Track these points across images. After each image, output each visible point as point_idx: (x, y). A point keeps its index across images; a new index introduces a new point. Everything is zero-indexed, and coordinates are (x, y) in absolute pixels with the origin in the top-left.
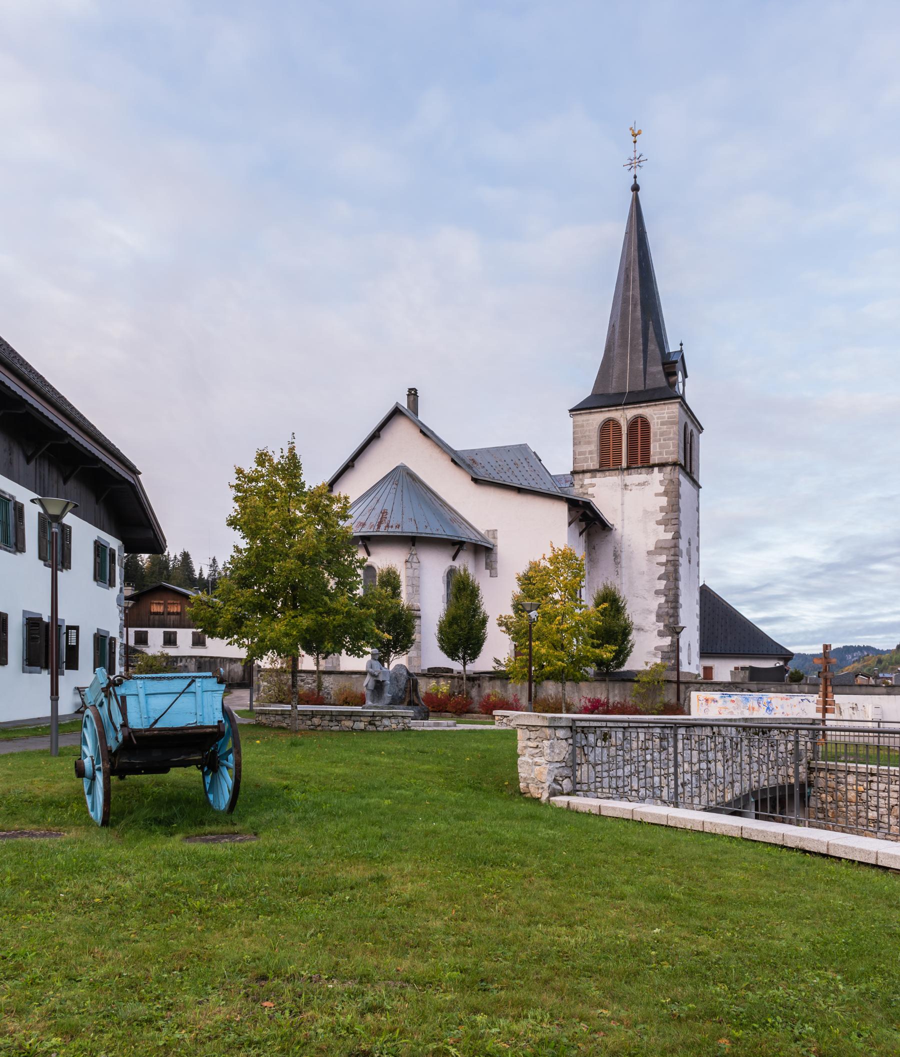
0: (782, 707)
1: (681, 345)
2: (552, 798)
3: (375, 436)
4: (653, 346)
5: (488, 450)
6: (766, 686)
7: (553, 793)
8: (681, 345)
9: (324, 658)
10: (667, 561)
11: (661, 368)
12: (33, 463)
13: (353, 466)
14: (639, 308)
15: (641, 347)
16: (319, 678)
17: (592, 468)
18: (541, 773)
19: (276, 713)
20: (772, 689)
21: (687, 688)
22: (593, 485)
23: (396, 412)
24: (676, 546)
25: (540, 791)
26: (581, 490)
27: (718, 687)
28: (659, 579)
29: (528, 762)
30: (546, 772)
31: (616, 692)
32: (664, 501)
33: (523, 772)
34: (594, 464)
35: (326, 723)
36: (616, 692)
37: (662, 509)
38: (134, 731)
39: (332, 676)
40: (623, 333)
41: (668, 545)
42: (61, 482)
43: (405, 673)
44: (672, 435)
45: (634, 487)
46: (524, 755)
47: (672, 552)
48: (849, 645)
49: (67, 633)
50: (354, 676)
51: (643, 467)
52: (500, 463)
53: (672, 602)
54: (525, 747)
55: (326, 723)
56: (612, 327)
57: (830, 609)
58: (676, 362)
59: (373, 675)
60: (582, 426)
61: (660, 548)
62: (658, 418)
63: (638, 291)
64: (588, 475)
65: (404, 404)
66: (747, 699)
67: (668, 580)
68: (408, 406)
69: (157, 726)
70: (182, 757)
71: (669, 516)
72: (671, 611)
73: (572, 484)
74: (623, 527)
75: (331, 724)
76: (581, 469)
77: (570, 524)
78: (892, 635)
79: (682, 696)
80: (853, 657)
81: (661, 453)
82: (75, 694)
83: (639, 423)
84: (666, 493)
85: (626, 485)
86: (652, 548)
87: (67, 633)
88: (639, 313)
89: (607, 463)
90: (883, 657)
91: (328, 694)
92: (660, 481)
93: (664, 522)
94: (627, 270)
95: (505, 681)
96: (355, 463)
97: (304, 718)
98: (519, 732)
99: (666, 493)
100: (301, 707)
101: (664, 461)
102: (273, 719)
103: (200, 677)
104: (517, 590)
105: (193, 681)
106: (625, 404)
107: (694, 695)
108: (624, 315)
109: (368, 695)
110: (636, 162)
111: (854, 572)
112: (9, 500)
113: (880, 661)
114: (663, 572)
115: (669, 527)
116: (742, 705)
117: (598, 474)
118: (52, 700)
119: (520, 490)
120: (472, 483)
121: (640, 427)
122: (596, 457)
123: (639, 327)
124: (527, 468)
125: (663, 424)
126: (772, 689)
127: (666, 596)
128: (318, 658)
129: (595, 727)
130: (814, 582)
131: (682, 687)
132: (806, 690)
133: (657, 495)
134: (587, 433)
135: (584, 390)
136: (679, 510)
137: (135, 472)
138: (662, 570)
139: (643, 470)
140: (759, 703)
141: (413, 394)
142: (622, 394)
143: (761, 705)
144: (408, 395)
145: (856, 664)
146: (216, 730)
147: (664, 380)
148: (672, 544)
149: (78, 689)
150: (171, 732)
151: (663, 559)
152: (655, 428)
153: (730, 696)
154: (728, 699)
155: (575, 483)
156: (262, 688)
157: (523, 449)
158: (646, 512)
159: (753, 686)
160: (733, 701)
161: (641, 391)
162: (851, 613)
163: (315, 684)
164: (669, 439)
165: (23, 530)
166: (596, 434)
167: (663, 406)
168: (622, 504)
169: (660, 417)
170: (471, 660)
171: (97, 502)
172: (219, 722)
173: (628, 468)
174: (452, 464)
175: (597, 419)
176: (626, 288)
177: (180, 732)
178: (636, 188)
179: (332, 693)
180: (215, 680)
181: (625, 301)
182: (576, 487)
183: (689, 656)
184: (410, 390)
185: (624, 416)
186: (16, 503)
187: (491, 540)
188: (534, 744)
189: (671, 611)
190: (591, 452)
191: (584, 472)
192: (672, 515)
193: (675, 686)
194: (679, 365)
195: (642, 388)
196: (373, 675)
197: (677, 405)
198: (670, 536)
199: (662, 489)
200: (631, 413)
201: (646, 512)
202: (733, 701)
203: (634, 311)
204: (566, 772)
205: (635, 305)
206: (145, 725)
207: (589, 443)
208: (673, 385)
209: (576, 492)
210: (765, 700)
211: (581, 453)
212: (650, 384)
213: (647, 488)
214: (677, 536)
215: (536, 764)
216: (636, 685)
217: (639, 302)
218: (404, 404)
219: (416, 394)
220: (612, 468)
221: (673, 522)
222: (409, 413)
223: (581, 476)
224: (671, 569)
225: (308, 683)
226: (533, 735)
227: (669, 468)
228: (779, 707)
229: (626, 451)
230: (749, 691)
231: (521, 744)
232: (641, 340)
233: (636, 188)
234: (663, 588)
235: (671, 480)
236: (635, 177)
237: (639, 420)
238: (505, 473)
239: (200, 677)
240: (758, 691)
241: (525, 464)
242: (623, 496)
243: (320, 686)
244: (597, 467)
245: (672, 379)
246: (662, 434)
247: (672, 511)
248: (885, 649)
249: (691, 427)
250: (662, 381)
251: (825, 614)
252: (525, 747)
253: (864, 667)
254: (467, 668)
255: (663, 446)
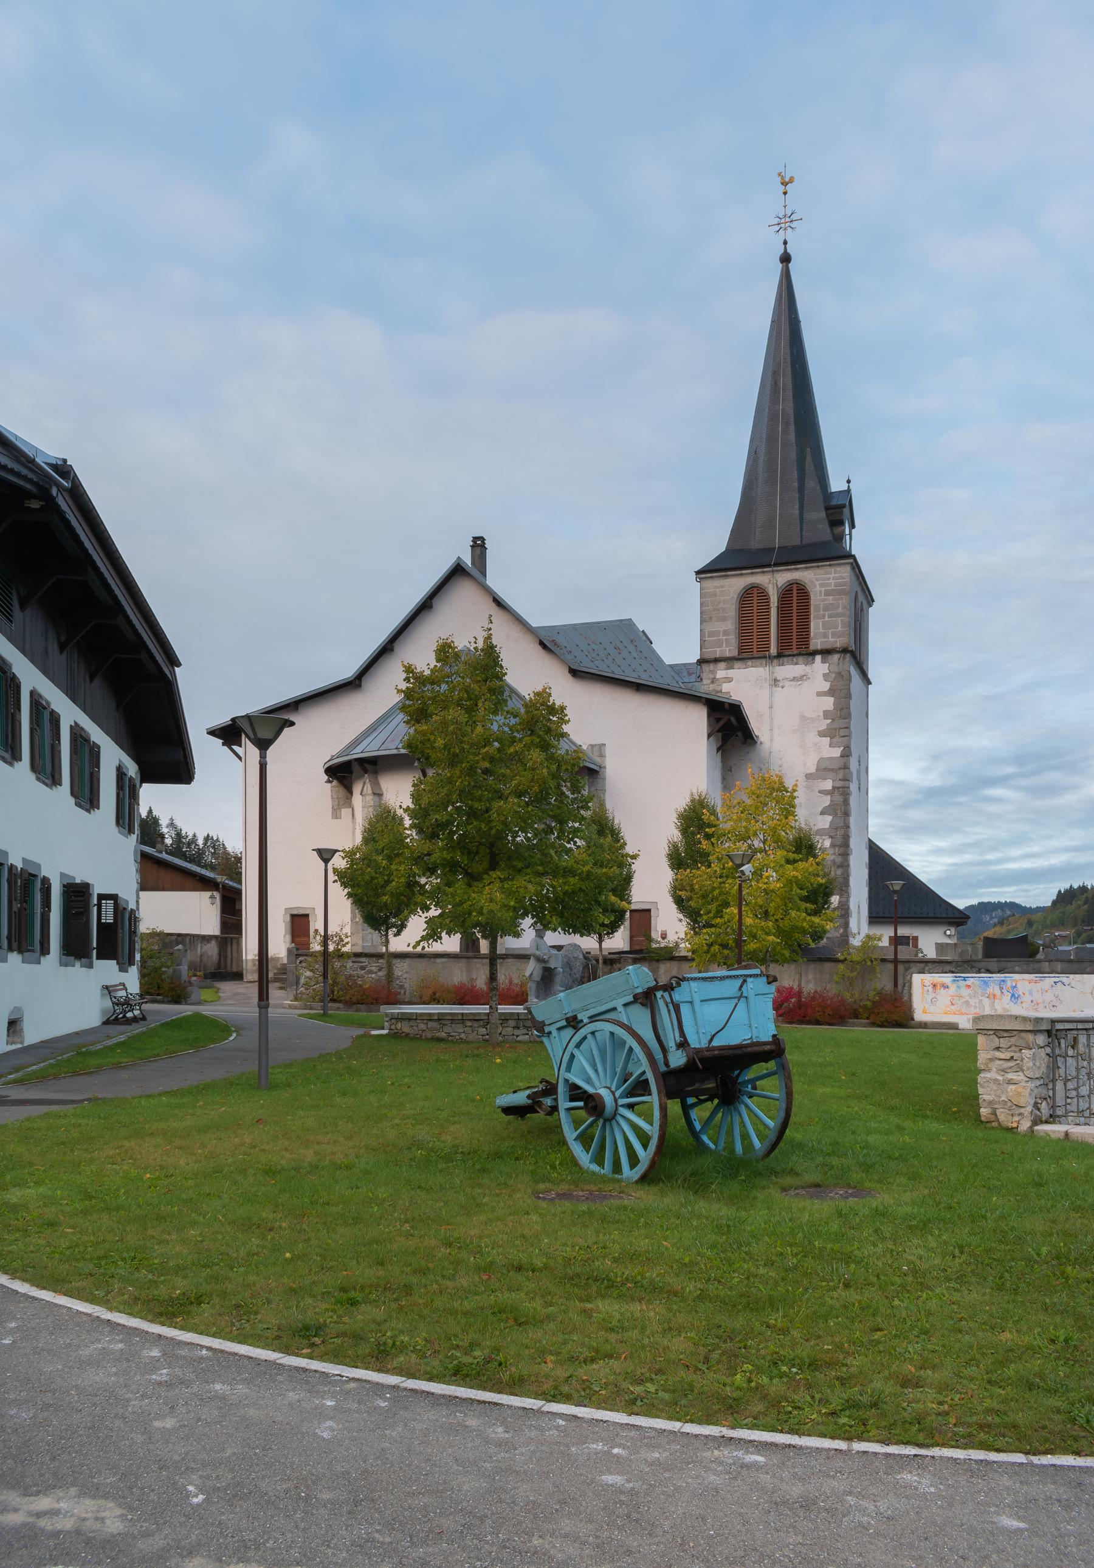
0: (1031, 993)
1: (849, 482)
2: (1036, 1128)
3: (426, 606)
4: (811, 483)
5: (575, 627)
6: (1009, 965)
7: (1037, 1121)
8: (849, 482)
9: (395, 935)
10: (834, 788)
11: (823, 514)
12: (65, 653)
13: (392, 650)
14: (792, 428)
15: (796, 484)
16: (390, 966)
17: (728, 655)
18: (1019, 1094)
19: (429, 1018)
20: (1017, 969)
21: (907, 969)
22: (729, 680)
23: (457, 571)
24: (846, 767)
25: (1016, 1118)
26: (712, 687)
27: (948, 967)
28: (822, 813)
29: (996, 1080)
30: (1027, 1092)
31: (811, 976)
32: (829, 703)
33: (986, 1094)
34: (729, 649)
35: (509, 1030)
36: (811, 976)
37: (826, 715)
38: (697, 1051)
39: (408, 961)
40: (771, 462)
41: (835, 766)
42: (88, 680)
43: (581, 957)
44: (840, 610)
45: (787, 683)
46: (989, 1070)
47: (840, 776)
48: (986, 900)
49: (99, 906)
50: (439, 960)
51: (800, 654)
52: (595, 647)
53: (840, 846)
54: (991, 1060)
55: (509, 1030)
56: (753, 455)
57: (939, 851)
58: (844, 506)
59: (539, 960)
60: (715, 595)
61: (823, 769)
62: (821, 585)
63: (790, 404)
64: (722, 665)
65: (468, 560)
66: (986, 983)
67: (835, 814)
68: (473, 563)
69: (715, 1043)
70: (697, 1086)
71: (836, 725)
72: (839, 860)
73: (700, 679)
74: (771, 740)
75: (517, 1032)
76: (713, 657)
77: (709, 736)
78: (1025, 887)
79: (900, 981)
80: (991, 918)
81: (825, 635)
82: (103, 995)
83: (795, 592)
84: (831, 692)
85: (776, 680)
86: (813, 770)
87: (99, 906)
88: (792, 436)
89: (750, 650)
90: (1034, 917)
91: (402, 987)
92: (824, 675)
93: (827, 733)
94: (775, 374)
95: (654, 963)
96: (396, 645)
97: (476, 1024)
98: (981, 1040)
99: (831, 692)
100: (504, 1009)
101: (829, 647)
102: (422, 1026)
103: (751, 976)
104: (676, 835)
105: (745, 981)
106: (776, 565)
107: (917, 979)
108: (771, 439)
109: (531, 987)
110: (786, 221)
111: (962, 799)
112: (45, 708)
113: (1030, 923)
114: (827, 803)
115: (836, 739)
116: (980, 991)
117: (737, 664)
118: (260, 1007)
119: (639, 688)
120: (569, 676)
121: (796, 599)
122: (733, 639)
123: (793, 455)
124: (634, 654)
125: (827, 593)
126: (1017, 969)
127: (832, 837)
128: (387, 935)
129: (1066, 1030)
130: (914, 814)
131: (901, 968)
132: (1059, 970)
133: (820, 694)
134: (722, 605)
135: (715, 542)
136: (848, 716)
137: (174, 662)
138: (827, 801)
139: (801, 658)
140: (1001, 988)
141: (479, 545)
142: (769, 551)
143: (1005, 991)
144: (472, 547)
145: (998, 928)
146: (773, 1047)
147: (829, 531)
148: (840, 763)
149: (107, 987)
150: (731, 1052)
151: (828, 785)
152: (817, 598)
153: (965, 979)
154: (962, 983)
155: (704, 676)
156: (302, 981)
157: (627, 626)
158: (803, 718)
159: (993, 963)
160: (969, 986)
161: (795, 547)
162: (968, 857)
163: (380, 974)
164: (837, 615)
165: (60, 752)
166: (733, 607)
167: (829, 569)
168: (771, 707)
169: (822, 582)
170: (608, 934)
171: (118, 708)
172: (774, 1036)
173: (780, 656)
174: (539, 648)
175: (734, 585)
176: (775, 400)
177: (739, 1052)
178: (786, 259)
179: (407, 985)
180: (764, 979)
181: (773, 417)
182: (705, 681)
183: (859, 922)
184: (475, 539)
185: (773, 581)
186: (53, 712)
187: (597, 759)
188: (1008, 1055)
189: (839, 860)
190: (726, 633)
191: (716, 660)
192: (841, 723)
193: (891, 966)
194: (846, 511)
195: (797, 542)
196: (539, 960)
197: (848, 568)
198: (837, 752)
199: (826, 686)
200: (785, 577)
201: (803, 718)
202: (969, 986)
203: (785, 432)
204: (1043, 1092)
205: (786, 425)
206: (704, 1044)
207: (724, 619)
208: (840, 538)
209: (705, 688)
210: (1009, 984)
211: (712, 634)
212: (809, 537)
213: (806, 684)
214: (846, 754)
215: (1010, 1082)
216: (841, 966)
217: (792, 420)
218: (468, 560)
219: (483, 546)
220: (755, 654)
221: (843, 732)
222: (475, 572)
223: (712, 666)
224: (839, 799)
225: (371, 972)
226: (1004, 1043)
227: (836, 657)
228: (1027, 993)
229: (776, 630)
230: (988, 971)
231: (983, 1057)
232: (795, 475)
233: (786, 259)
234: (827, 826)
235: (839, 673)
236: (785, 243)
237: (795, 586)
238: (611, 659)
239: (751, 976)
240: (999, 972)
241: (631, 648)
242: (771, 695)
243: (390, 976)
244: (735, 653)
245: (838, 530)
246: (827, 608)
247: (841, 717)
248: (1034, 906)
249: (861, 598)
250: (824, 532)
251: (932, 858)
252: (991, 1060)
253: (1009, 931)
254: (604, 945)
255: (824, 629)
